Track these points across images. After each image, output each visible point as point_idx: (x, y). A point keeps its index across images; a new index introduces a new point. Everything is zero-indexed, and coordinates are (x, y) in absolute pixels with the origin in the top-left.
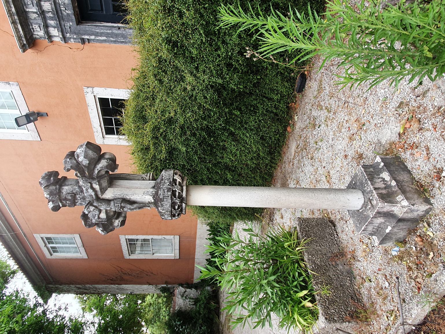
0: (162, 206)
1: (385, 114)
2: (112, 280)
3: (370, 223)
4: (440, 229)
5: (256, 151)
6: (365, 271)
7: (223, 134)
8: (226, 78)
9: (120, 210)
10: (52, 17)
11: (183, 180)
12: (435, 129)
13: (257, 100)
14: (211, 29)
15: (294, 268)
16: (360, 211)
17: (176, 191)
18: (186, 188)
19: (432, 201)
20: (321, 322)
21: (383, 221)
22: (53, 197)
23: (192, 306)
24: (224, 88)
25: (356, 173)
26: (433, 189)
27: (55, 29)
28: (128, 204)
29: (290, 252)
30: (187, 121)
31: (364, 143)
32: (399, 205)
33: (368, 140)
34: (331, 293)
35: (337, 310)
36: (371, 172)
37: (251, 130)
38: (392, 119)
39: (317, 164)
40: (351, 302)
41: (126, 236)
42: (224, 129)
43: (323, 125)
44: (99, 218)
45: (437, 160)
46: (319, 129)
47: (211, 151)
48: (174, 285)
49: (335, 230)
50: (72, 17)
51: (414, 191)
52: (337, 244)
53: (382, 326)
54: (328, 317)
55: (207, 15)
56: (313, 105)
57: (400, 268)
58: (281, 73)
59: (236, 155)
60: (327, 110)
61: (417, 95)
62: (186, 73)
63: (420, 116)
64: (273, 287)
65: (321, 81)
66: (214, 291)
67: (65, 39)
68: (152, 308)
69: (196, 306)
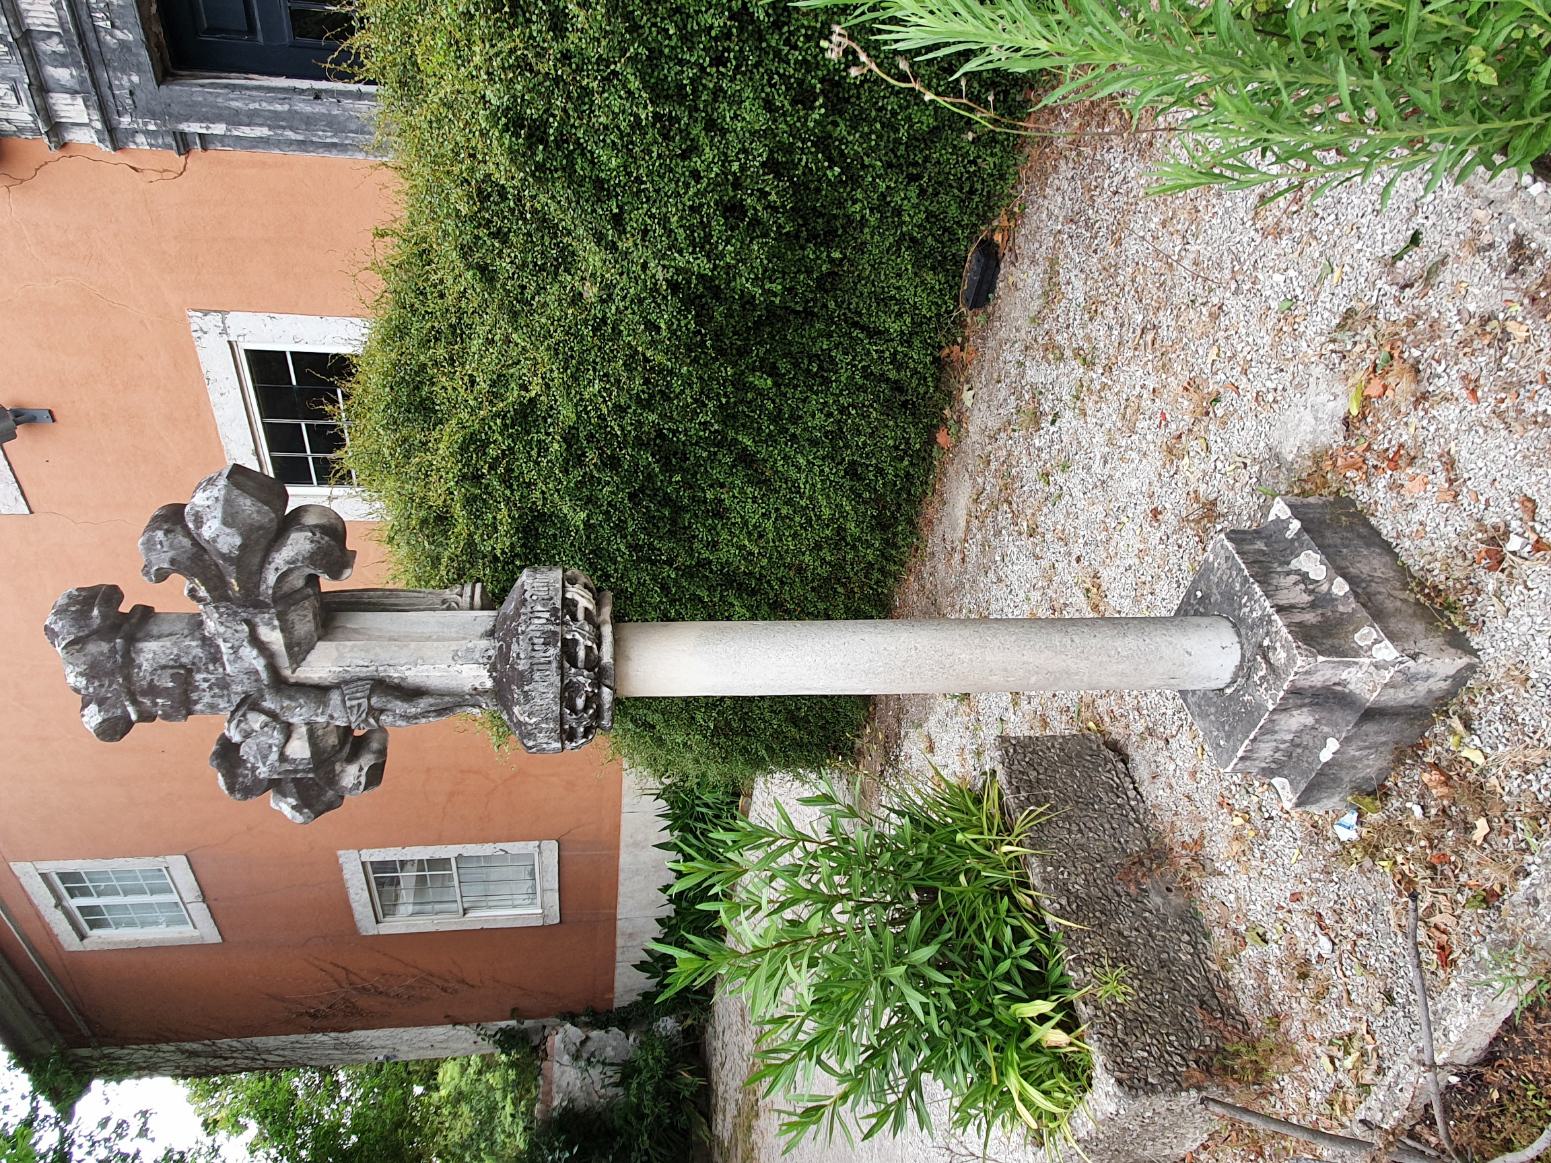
0: (527, 701)
1: (1290, 356)
2: (314, 1016)
3: (1264, 731)
4: (1507, 735)
5: (832, 520)
6: (1244, 906)
7: (712, 457)
8: (722, 256)
9: (366, 721)
10: (63, 55)
11: (599, 604)
12: (1473, 392)
13: (829, 336)
14: (666, 77)
15: (996, 912)
16: (1228, 691)
17: (575, 642)
18: (614, 633)
19: (1475, 640)
20: (1104, 1096)
21: (1309, 720)
22: (101, 686)
23: (611, 1091)
24: (716, 293)
25: (1206, 561)
26: (1475, 601)
27: (74, 99)
28: (397, 698)
29: (980, 857)
30: (587, 413)
31: (1219, 464)
32: (1367, 661)
33: (1234, 450)
34: (1130, 990)
35: (1154, 1050)
36: (1262, 553)
37: (814, 443)
38: (1318, 370)
39: (1053, 551)
40: (1200, 1017)
41: (363, 852)
42: (721, 442)
43: (1068, 414)
44: (283, 758)
45: (1487, 500)
46: (1052, 429)
47: (674, 522)
48: (544, 1021)
49: (1128, 774)
50: (139, 55)
51: (1410, 611)
52: (1137, 820)
53: (1312, 1094)
54: (1125, 1076)
55: (654, 25)
56: (1027, 348)
57: (1375, 885)
58: (913, 240)
59: (761, 536)
60: (1079, 361)
61: (1402, 282)
62: (579, 240)
63: (1416, 353)
64: (926, 986)
65: (1053, 262)
66: (687, 1033)
67: (114, 136)
68: (464, 1108)
69: (627, 1089)
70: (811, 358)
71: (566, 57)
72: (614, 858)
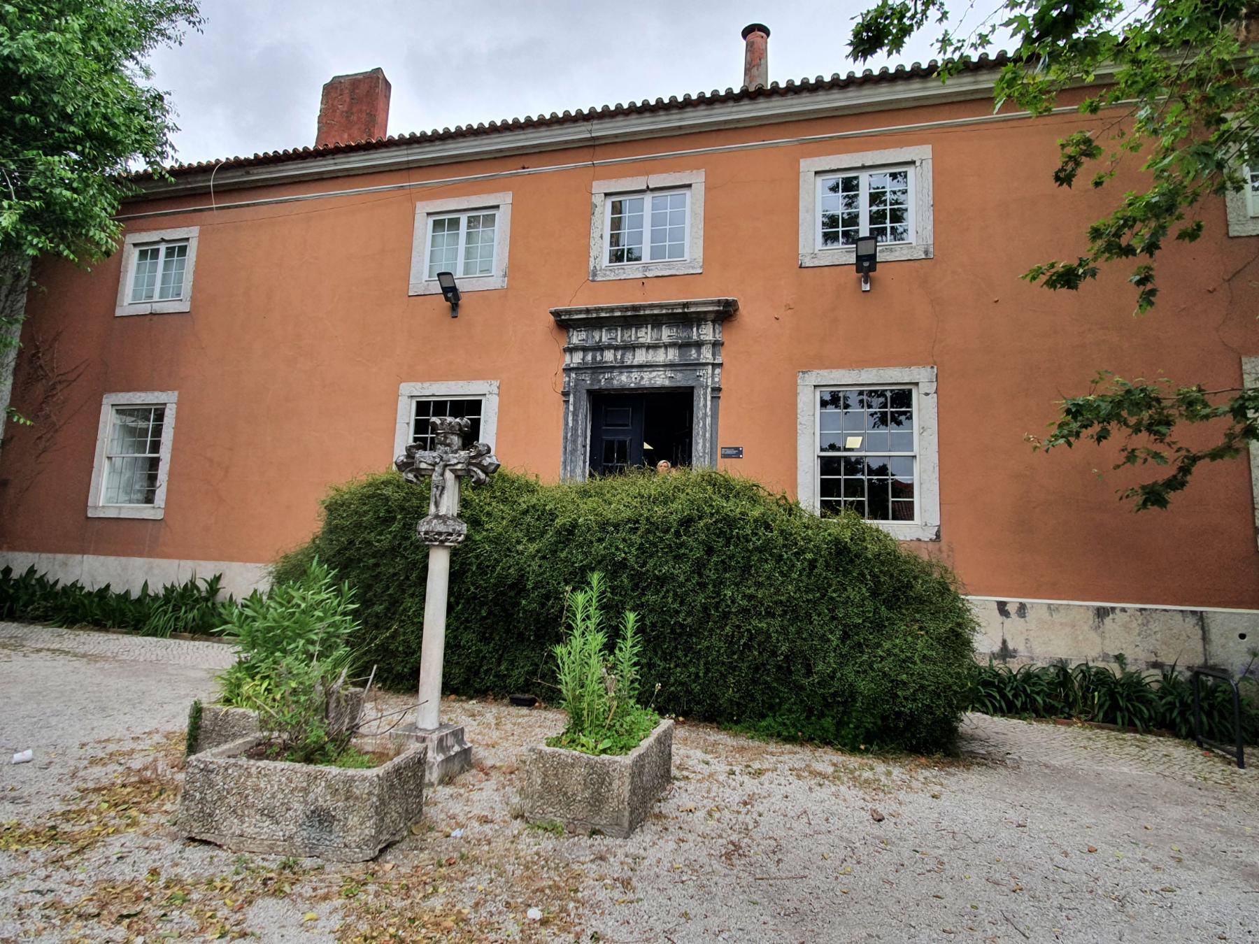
67: (568, 370)
70: (491, 634)
71: (592, 542)
72: (140, 554)
